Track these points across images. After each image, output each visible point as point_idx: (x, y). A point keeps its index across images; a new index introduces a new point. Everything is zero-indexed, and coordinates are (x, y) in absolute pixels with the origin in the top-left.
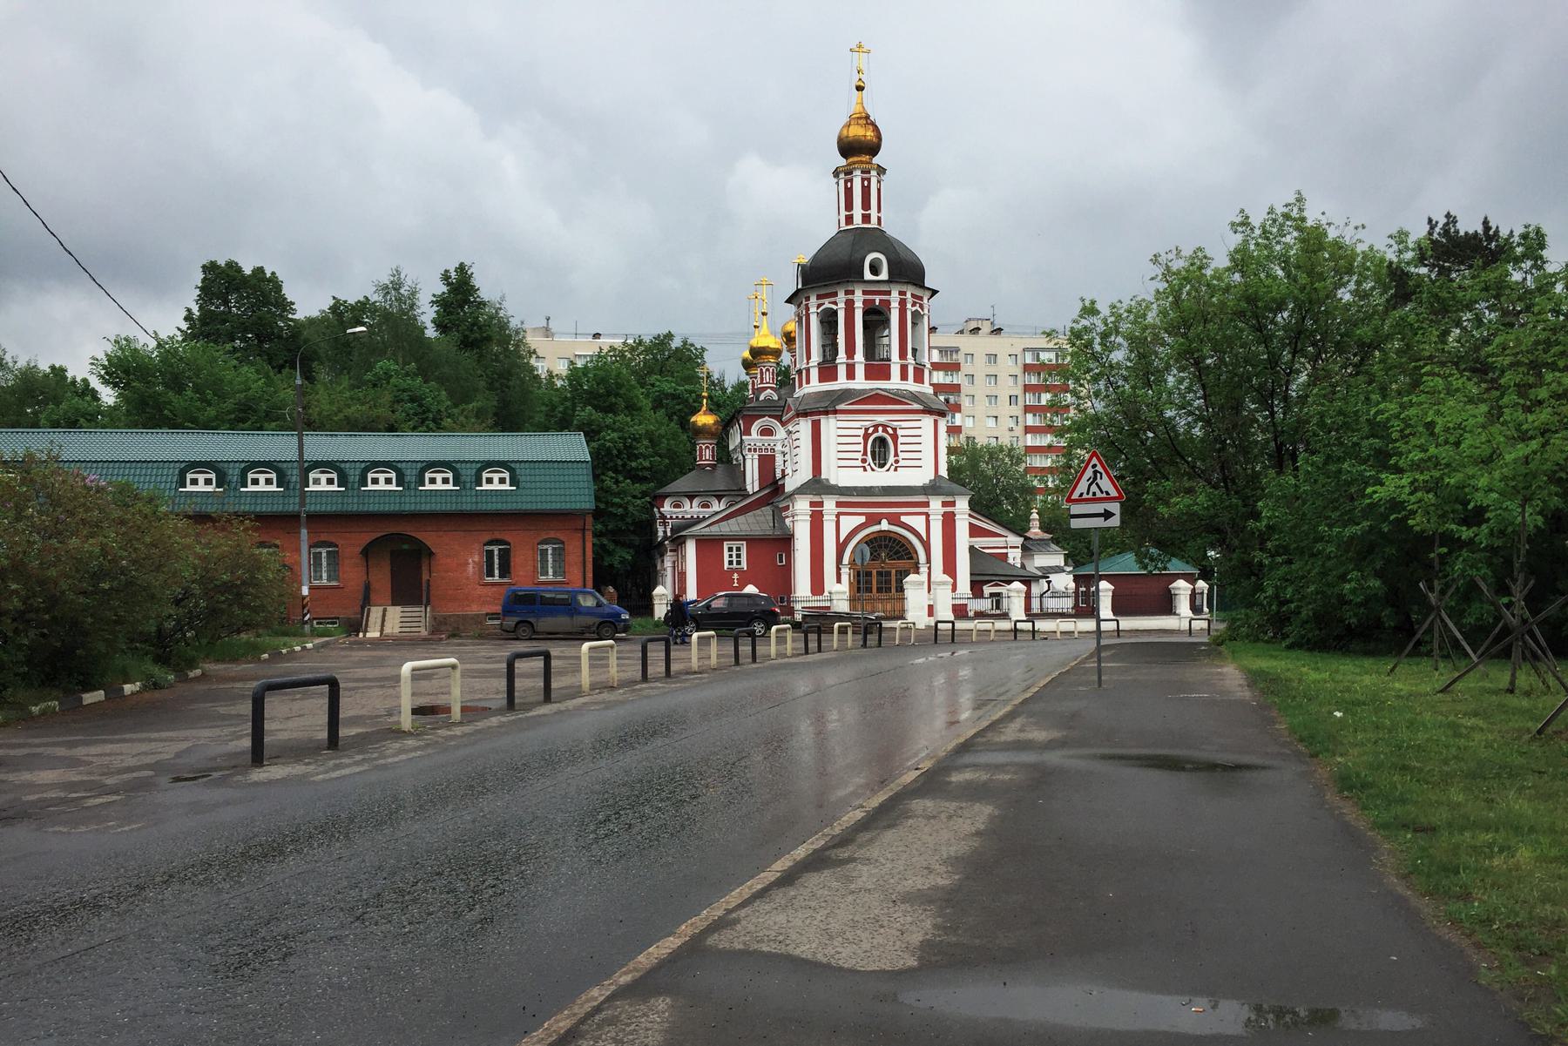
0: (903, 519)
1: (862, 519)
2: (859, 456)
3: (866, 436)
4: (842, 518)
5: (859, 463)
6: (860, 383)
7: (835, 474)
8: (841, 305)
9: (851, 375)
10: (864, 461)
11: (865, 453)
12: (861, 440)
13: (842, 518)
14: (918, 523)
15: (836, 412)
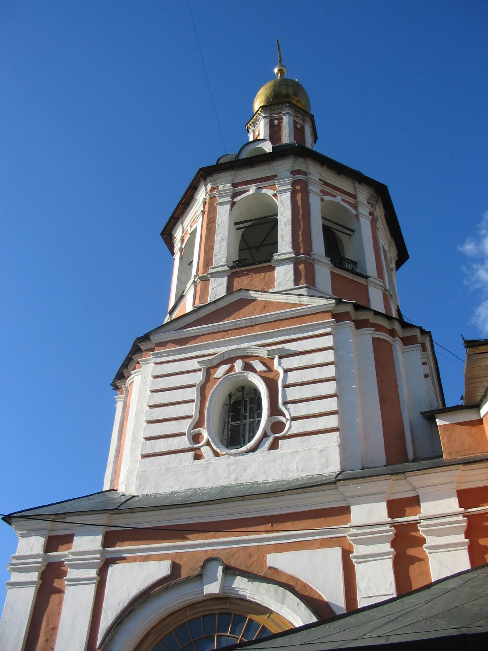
0: (274, 560)
1: (161, 569)
2: (185, 426)
5: (184, 442)
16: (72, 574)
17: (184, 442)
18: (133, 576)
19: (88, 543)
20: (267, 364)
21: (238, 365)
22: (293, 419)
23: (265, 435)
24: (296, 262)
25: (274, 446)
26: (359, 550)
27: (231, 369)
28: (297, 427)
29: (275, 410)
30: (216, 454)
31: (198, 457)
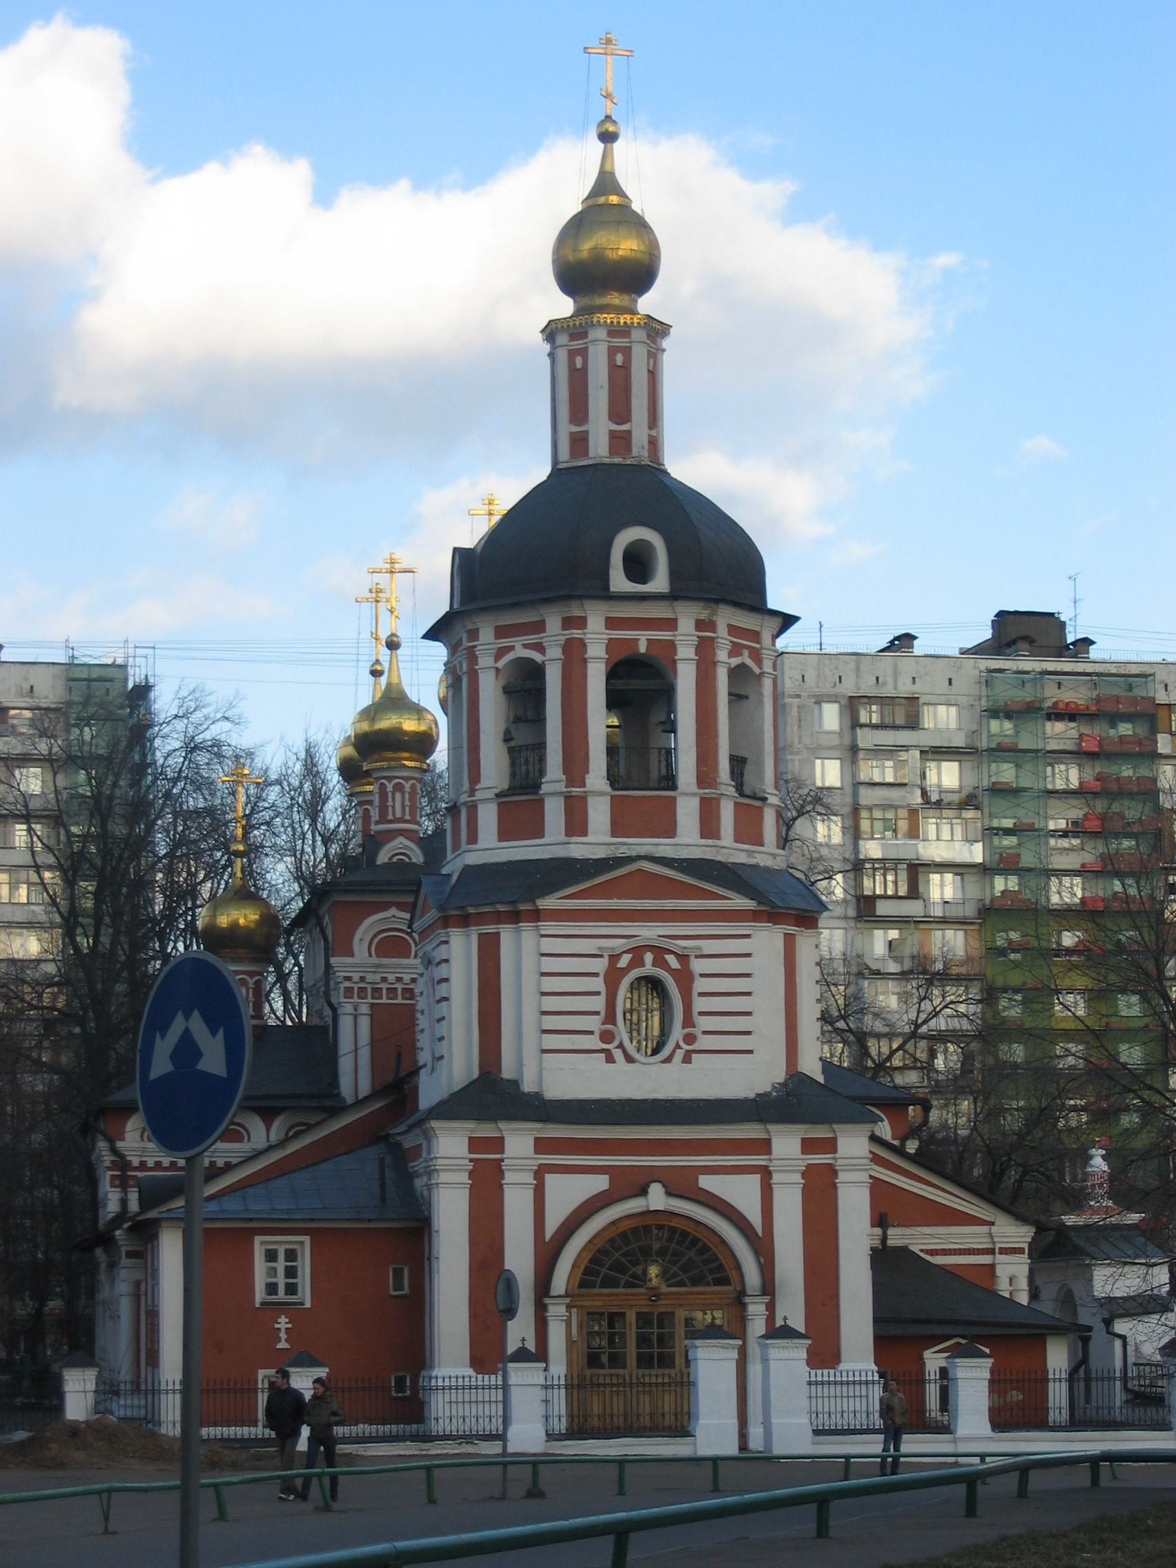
0: (705, 1182)
1: (601, 1183)
2: (594, 1023)
4: (549, 1178)
6: (598, 840)
8: (554, 652)
10: (607, 1037)
11: (610, 1017)
12: (598, 984)
13: (549, 1178)
14: (741, 1192)
16: (842, 1177)
17: (594, 1042)
18: (567, 1193)
20: (683, 958)
21: (649, 957)
22: (705, 1033)
23: (678, 1046)
24: (568, 798)
25: (687, 1059)
26: (776, 1178)
28: (704, 1042)
29: (688, 1021)
30: (629, 1059)
31: (610, 1059)
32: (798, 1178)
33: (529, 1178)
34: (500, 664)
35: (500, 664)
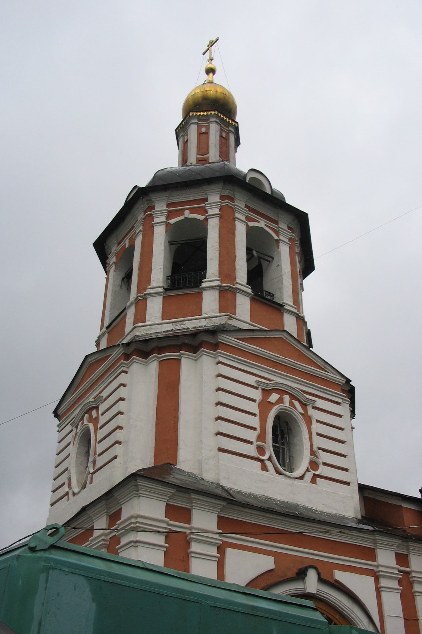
0: (340, 576)
1: (267, 563)
2: (252, 436)
3: (265, 406)
5: (251, 450)
7: (199, 455)
9: (227, 295)
11: (261, 437)
13: (230, 552)
15: (215, 346)
16: (195, 547)
17: (251, 450)
19: (204, 520)
25: (313, 481)
26: (383, 582)
27: (280, 401)
31: (264, 468)
32: (160, 540)
33: (213, 551)
34: (172, 221)
35: (172, 221)
